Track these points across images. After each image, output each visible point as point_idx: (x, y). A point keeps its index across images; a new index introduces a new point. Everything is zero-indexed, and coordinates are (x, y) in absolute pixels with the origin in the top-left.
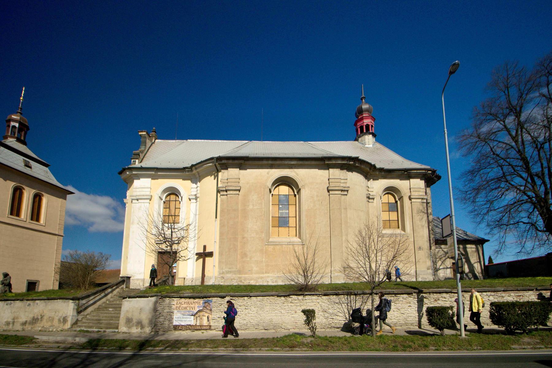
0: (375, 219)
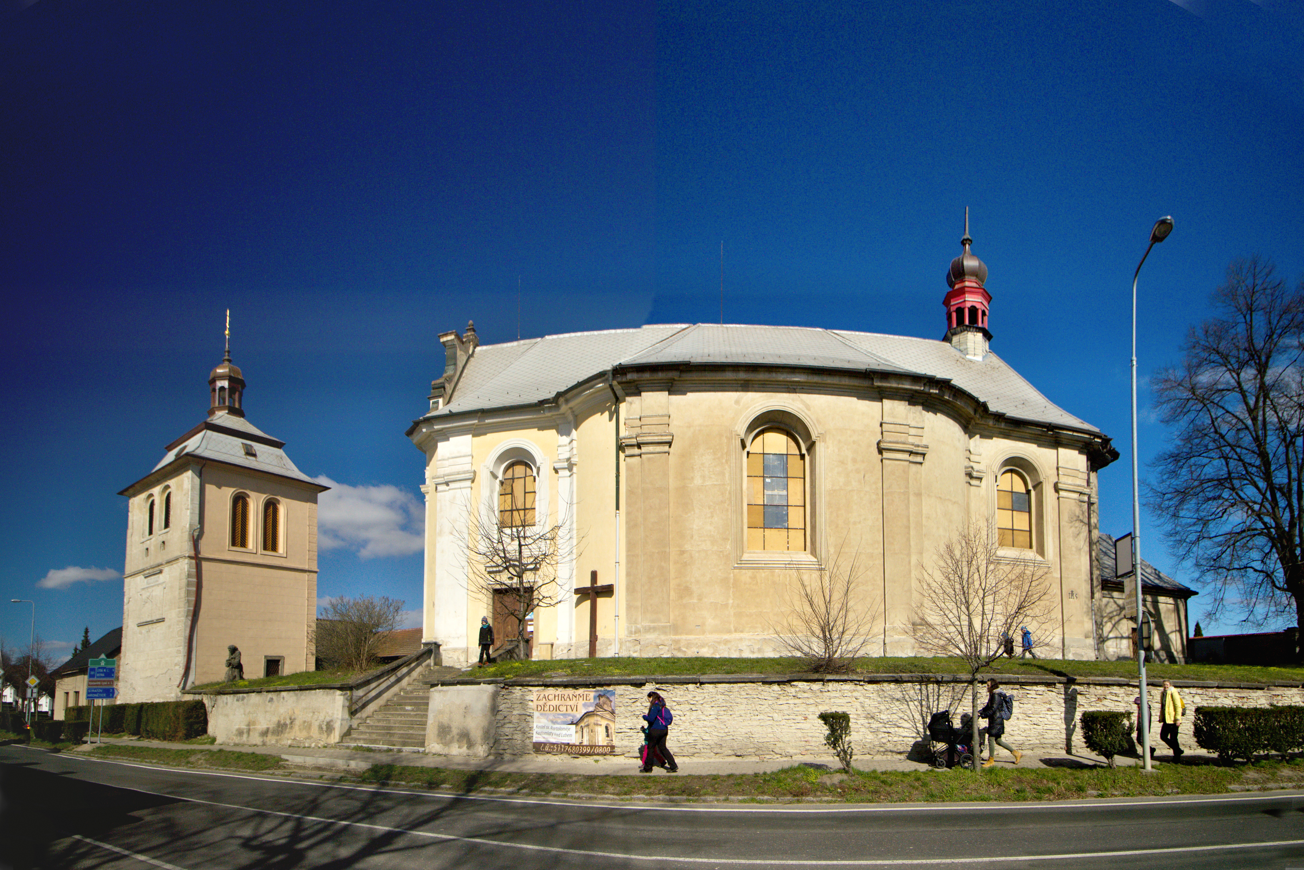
0: (983, 524)
